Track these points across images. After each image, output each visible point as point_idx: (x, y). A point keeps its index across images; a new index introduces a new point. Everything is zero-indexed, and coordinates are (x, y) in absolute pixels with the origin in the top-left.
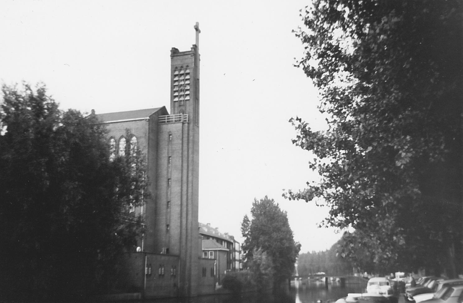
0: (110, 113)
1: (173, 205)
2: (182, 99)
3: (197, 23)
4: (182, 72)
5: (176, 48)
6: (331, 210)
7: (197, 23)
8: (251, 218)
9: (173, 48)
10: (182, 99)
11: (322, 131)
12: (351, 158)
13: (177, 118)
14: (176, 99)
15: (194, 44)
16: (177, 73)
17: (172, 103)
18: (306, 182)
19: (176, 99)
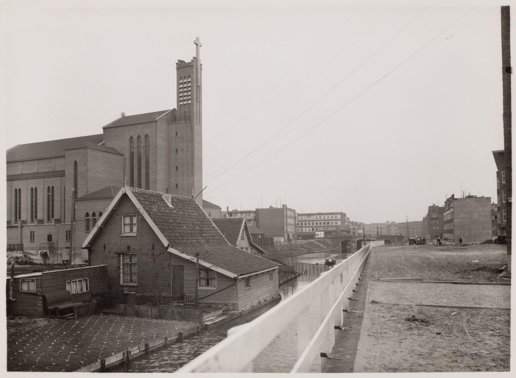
0: (202, 166)
1: (477, 267)
2: (185, 103)
3: (197, 39)
4: (185, 81)
5: (182, 60)
6: (346, 217)
7: (197, 39)
8: (390, 222)
9: (179, 61)
10: (185, 103)
11: (259, 226)
12: (196, 259)
13: (314, 271)
14: (181, 103)
15: (195, 56)
16: (181, 81)
17: (179, 106)
18: (505, 4)
19: (181, 103)
